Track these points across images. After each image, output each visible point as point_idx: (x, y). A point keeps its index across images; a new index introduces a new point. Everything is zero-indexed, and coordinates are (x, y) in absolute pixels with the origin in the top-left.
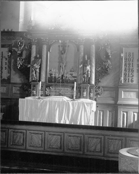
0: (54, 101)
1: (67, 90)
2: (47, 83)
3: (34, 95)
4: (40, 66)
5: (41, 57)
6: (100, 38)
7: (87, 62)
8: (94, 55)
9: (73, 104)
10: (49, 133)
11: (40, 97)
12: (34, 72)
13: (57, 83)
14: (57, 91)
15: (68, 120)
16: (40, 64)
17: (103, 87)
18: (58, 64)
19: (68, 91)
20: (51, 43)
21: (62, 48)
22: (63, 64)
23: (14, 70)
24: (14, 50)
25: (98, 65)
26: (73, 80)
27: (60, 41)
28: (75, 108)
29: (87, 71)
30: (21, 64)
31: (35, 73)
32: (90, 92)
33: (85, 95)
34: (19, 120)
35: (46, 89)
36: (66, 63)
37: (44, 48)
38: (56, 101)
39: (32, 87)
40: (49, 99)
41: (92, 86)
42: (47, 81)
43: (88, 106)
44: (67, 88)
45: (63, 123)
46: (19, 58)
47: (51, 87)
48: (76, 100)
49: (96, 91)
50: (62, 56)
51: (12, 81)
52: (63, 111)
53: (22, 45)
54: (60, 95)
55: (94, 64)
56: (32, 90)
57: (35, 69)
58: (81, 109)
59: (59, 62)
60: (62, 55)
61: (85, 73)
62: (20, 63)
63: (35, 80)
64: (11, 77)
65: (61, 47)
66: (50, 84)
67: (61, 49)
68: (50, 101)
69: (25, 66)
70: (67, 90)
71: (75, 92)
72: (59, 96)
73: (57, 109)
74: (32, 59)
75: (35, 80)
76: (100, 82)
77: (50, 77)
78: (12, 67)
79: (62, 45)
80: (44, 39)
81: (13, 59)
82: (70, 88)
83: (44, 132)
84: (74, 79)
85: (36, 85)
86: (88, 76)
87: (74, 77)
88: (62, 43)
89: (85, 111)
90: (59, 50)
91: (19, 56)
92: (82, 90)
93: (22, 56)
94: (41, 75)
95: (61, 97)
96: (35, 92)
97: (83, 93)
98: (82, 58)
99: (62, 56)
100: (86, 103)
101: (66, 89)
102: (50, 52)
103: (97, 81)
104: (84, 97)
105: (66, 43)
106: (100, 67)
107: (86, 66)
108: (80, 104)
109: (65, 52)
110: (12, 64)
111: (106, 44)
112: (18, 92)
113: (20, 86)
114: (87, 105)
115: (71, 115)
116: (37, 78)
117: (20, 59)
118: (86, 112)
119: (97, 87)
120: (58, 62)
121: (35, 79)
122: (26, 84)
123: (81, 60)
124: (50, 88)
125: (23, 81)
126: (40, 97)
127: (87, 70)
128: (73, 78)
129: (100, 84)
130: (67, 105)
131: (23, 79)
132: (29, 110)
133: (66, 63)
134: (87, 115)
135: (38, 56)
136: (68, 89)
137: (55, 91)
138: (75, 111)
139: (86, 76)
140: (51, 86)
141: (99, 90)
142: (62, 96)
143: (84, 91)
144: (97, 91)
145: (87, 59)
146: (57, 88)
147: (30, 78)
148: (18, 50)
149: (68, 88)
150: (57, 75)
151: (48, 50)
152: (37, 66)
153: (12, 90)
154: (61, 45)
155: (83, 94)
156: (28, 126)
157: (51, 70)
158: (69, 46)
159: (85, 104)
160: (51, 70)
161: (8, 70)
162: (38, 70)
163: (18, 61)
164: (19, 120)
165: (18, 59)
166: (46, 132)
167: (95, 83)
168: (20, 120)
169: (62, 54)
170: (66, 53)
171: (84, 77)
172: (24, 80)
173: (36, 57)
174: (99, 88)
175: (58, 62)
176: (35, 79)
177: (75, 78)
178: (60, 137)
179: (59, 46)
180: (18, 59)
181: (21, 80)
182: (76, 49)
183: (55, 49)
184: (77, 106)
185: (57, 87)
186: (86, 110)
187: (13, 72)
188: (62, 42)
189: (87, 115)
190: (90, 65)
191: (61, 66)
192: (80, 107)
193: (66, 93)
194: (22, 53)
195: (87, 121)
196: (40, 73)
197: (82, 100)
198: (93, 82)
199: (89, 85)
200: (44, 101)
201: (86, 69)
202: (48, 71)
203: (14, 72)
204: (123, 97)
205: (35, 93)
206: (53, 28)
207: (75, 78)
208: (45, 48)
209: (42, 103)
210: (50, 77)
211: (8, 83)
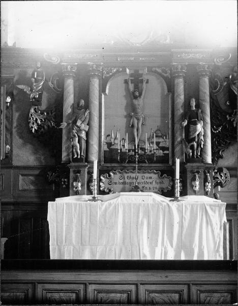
0: (135, 204)
1: (151, 178)
2: (103, 163)
3: (77, 193)
4: (88, 125)
5: (87, 106)
6: (217, 63)
7: (197, 114)
8: (208, 99)
9: (180, 211)
10: (199, 288)
11: (96, 196)
12: (77, 139)
13: (129, 162)
14: (127, 181)
15: (172, 246)
16: (87, 120)
17: (229, 169)
18: (125, 120)
19: (151, 180)
20: (108, 75)
21: (133, 85)
22: (138, 120)
23: (20, 138)
24: (22, 90)
25: (216, 121)
26: (161, 155)
27: (128, 71)
28: (186, 218)
29: (198, 135)
30: (39, 122)
31: (79, 142)
32: (206, 180)
33: (197, 188)
34: (51, 258)
35: (102, 178)
36: (144, 119)
37: (94, 85)
38: (140, 204)
39: (72, 175)
40: (122, 200)
41: (208, 169)
42: (102, 159)
43: (215, 212)
44: (149, 173)
45: (172, 259)
46: (35, 109)
47: (111, 174)
48: (181, 200)
49: (215, 178)
50: (135, 102)
51: (15, 163)
52: (159, 225)
53: (42, 80)
54: (136, 189)
55: (208, 120)
56: (71, 181)
57: (79, 130)
58: (198, 218)
59: (129, 117)
60: (134, 100)
61: (194, 139)
62: (36, 119)
63: (79, 157)
64: (14, 152)
65: (131, 83)
66: (109, 165)
67: (131, 87)
68: (124, 205)
69: (48, 126)
70: (151, 178)
71: (179, 181)
72: (134, 191)
73: (142, 223)
74: (67, 110)
75: (79, 157)
76: (221, 157)
77: (108, 149)
78: (14, 130)
79: (132, 78)
80: (95, 66)
81: (17, 111)
82: (155, 173)
83: (186, 286)
84: (164, 154)
85: (81, 169)
86: (199, 145)
87: (163, 149)
88: (131, 75)
89: (209, 222)
90: (127, 89)
91: (33, 104)
92: (189, 175)
93: (40, 105)
94: (90, 146)
95: (140, 193)
96: (80, 184)
97: (193, 184)
98: (182, 106)
99: (135, 102)
100: (210, 206)
101: (147, 175)
102: (105, 94)
103: (216, 156)
104: (195, 193)
105: (141, 75)
106: (220, 126)
107: (195, 124)
108: (197, 209)
109: (140, 94)
110: (15, 125)
111: (230, 77)
112: (32, 187)
113: (37, 172)
114: (212, 209)
115: (178, 235)
116: (82, 154)
117: (37, 110)
118: (209, 227)
119: (216, 168)
120: (126, 117)
121: (78, 155)
122: (53, 169)
123: (180, 111)
124: (110, 176)
125: (43, 161)
126: (96, 196)
127: (197, 133)
128: (161, 151)
129: (222, 163)
130: (167, 210)
131: (42, 157)
132: (74, 227)
133: (144, 119)
134: (213, 231)
135: (82, 102)
136: (152, 175)
137: (122, 181)
138: (186, 224)
139: (195, 144)
140: (113, 169)
141: (221, 176)
142: (142, 191)
143: (194, 179)
144: (218, 178)
145: (194, 108)
146: (126, 175)
147: (64, 154)
148: (31, 90)
149: (151, 173)
150: (122, 145)
151: (102, 90)
152: (83, 125)
153: (17, 180)
154: (130, 78)
155: (192, 186)
156: (178, 274)
157: (108, 136)
158: (148, 80)
159: (208, 208)
160: (108, 136)
161: (6, 137)
162: (83, 135)
163: (31, 115)
164: (51, 258)
165: (32, 111)
166: (193, 284)
167: (213, 160)
168: (52, 258)
169: (136, 98)
170: (142, 97)
171: (192, 147)
172: (45, 159)
173: (76, 107)
174: (220, 170)
175: (126, 117)
176: (78, 155)
177: (166, 152)
178: (230, 296)
179: (126, 82)
180: (32, 111)
181: (38, 159)
182: (166, 88)
183: (116, 91)
184: (188, 213)
185: (126, 173)
186: (211, 221)
187: (17, 141)
188: (132, 72)
189: (213, 231)
190: (202, 122)
191: (133, 126)
192: (197, 214)
193: (146, 186)
194: (40, 95)
195: (215, 243)
196: (87, 142)
197: (190, 199)
198: (209, 159)
199: (86, 164)
200: (110, 204)
201: (195, 130)
202: (103, 138)
203: (20, 141)
204: (219, 190)
205: (80, 189)
206: (113, 42)
207: (166, 152)
208: (96, 84)
209: (106, 210)
210: (108, 149)
211: (7, 168)
